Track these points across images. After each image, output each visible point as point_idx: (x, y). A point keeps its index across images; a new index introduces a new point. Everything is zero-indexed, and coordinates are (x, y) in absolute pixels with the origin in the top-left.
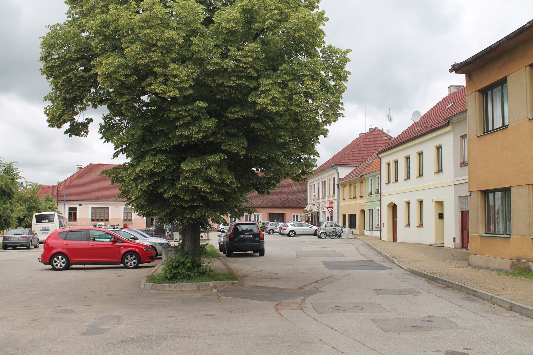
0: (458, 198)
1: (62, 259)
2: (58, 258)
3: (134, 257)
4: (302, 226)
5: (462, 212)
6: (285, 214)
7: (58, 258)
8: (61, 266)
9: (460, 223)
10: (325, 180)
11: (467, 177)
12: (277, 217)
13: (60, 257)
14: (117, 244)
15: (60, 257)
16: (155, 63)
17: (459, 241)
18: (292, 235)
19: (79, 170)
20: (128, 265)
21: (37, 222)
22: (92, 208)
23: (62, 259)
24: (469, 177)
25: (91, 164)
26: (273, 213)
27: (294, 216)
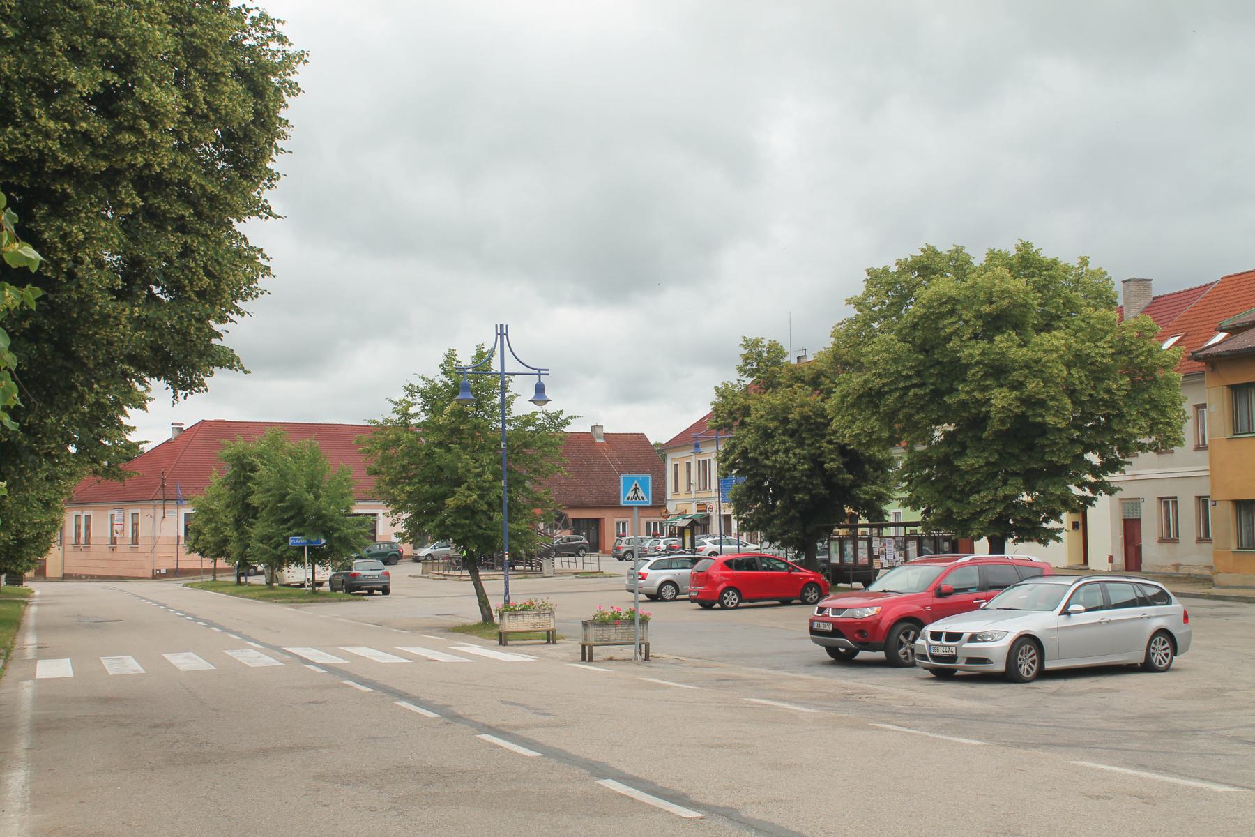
0: (1118, 501)
1: (728, 594)
2: (726, 598)
3: (808, 589)
4: (730, 544)
5: (1125, 521)
6: (602, 520)
7: (726, 598)
8: (732, 603)
9: (1122, 536)
10: (707, 458)
11: (1208, 468)
12: (586, 526)
13: (726, 595)
14: (792, 573)
15: (726, 595)
16: (217, 109)
17: (1120, 560)
18: (730, 605)
19: (177, 433)
20: (808, 600)
21: (991, 553)
22: (186, 514)
23: (728, 594)
24: (1212, 469)
25: (204, 421)
26: (578, 519)
27: (618, 524)
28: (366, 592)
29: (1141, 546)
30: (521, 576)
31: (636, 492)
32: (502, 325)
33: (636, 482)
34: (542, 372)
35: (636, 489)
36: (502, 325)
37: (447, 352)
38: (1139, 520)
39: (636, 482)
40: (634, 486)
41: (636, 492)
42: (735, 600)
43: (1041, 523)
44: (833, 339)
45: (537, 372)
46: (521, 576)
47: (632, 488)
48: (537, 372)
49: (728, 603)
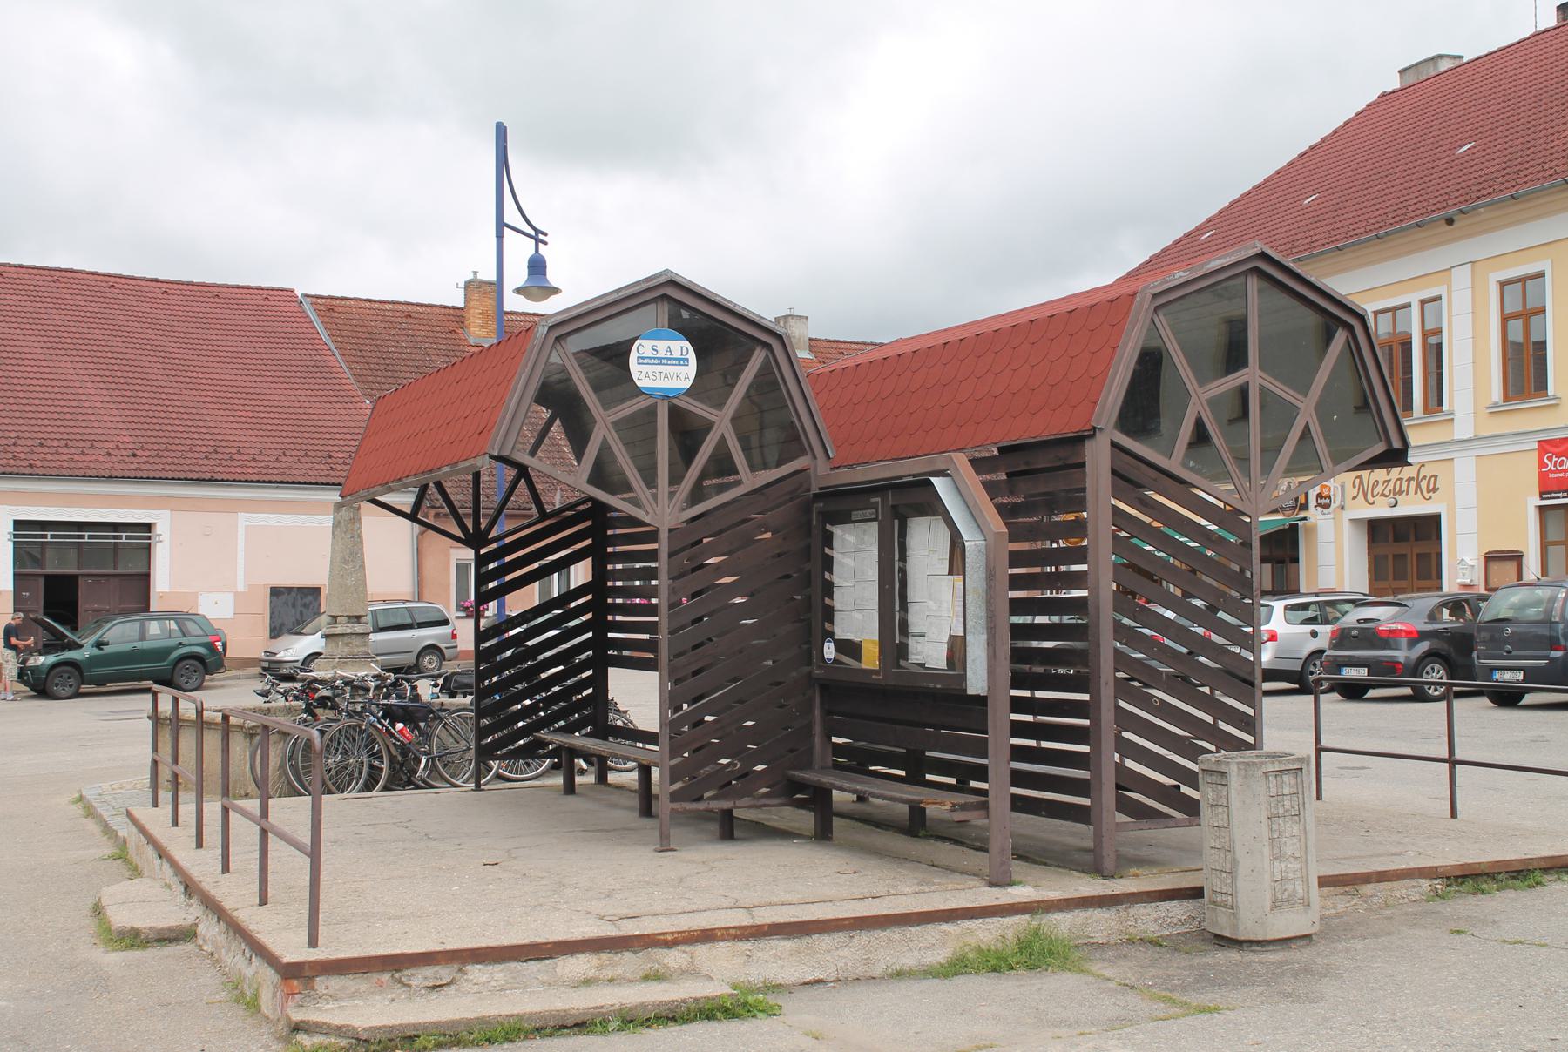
30: (985, 933)
46: (985, 933)
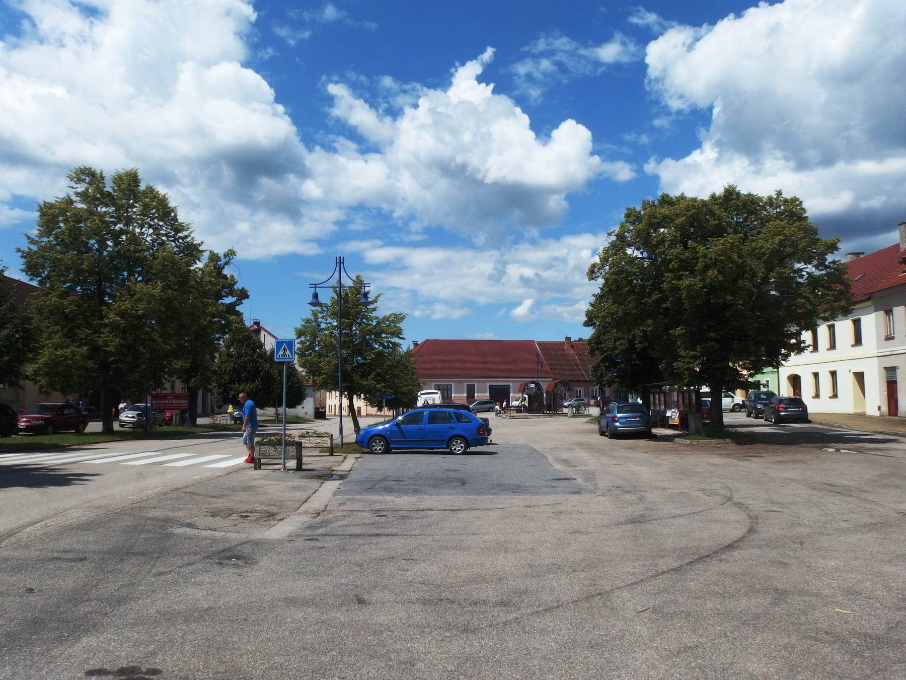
28: (594, 395)
29: (540, 344)
31: (285, 352)
32: (340, 257)
33: (285, 344)
34: (317, 286)
35: (285, 349)
36: (340, 257)
37: (642, 202)
38: (896, 381)
39: (285, 344)
40: (283, 347)
41: (285, 352)
42: (462, 447)
43: (150, 394)
44: (23, 260)
45: (314, 286)
47: (282, 348)
48: (314, 286)
49: (455, 449)
